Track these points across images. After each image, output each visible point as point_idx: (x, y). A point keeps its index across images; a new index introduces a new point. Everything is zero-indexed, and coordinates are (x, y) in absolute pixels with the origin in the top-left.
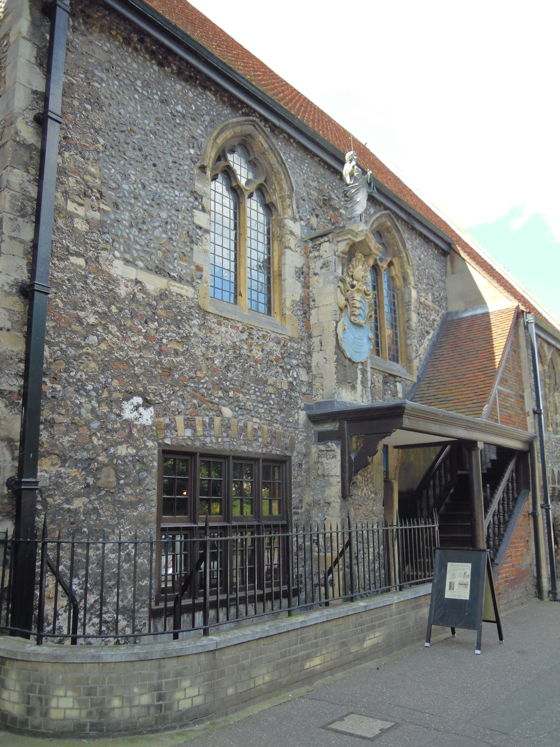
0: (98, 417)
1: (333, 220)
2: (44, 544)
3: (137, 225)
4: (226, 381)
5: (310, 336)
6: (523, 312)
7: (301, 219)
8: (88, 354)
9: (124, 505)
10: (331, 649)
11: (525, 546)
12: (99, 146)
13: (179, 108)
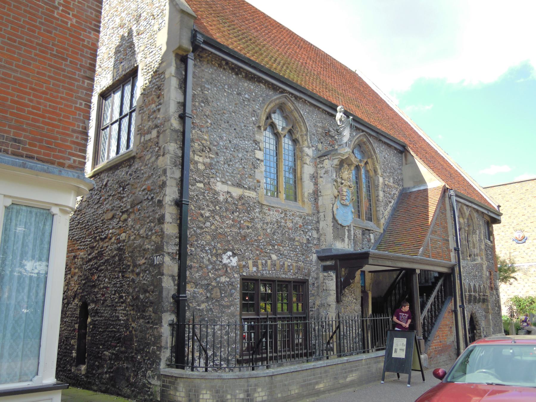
0: (211, 263)
1: (331, 143)
2: (194, 326)
3: (227, 162)
4: (273, 240)
5: (318, 212)
6: (448, 188)
7: (313, 146)
8: (206, 232)
9: (224, 307)
10: (329, 380)
11: (449, 330)
12: (208, 124)
13: (247, 96)
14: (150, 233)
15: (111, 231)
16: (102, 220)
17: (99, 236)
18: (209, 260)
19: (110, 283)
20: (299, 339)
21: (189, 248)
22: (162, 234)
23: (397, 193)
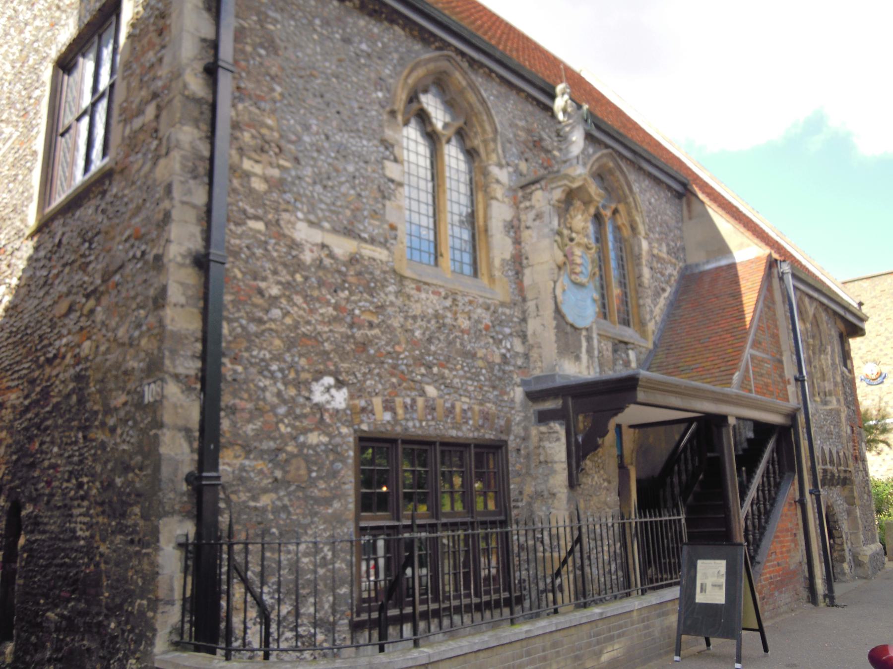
0: (284, 402)
1: (545, 164)
3: (321, 181)
4: (429, 355)
6: (776, 260)
7: (508, 165)
8: (271, 330)
9: (317, 501)
13: (364, 46)
14: (137, 334)
15: (64, 341)
16: (51, 320)
17: (44, 354)
18: (279, 394)
19: (61, 455)
20: (489, 566)
21: (229, 366)
22: (160, 332)
23: (675, 273)
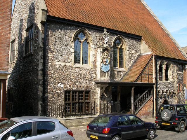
9: (58, 99)
